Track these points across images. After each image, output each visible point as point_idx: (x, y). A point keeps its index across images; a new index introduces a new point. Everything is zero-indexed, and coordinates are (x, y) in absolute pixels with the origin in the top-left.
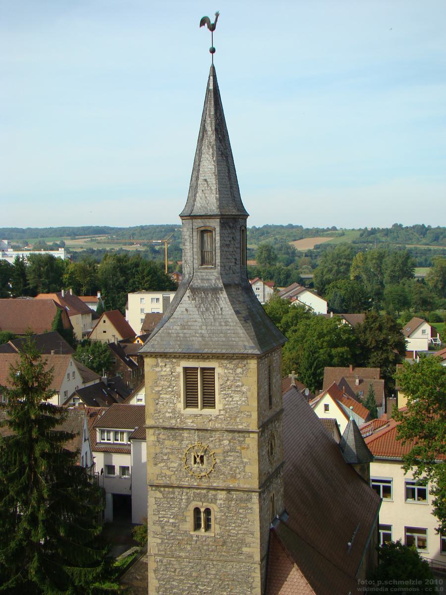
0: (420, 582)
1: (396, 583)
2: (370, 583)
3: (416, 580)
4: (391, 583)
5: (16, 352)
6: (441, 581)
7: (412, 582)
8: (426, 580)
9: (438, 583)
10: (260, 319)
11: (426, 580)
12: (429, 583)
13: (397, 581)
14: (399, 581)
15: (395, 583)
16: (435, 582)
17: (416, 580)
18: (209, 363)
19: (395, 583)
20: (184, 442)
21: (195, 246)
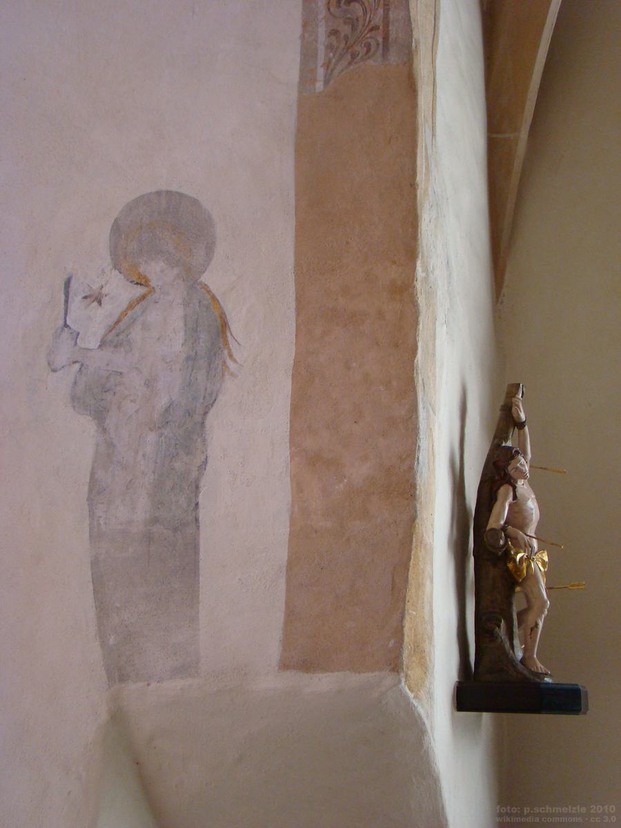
0: (584, 810)
1: (551, 811)
2: (503, 810)
3: (578, 806)
4: (543, 810)
5: (415, 40)
6: (612, 810)
7: (572, 809)
8: (592, 807)
9: (608, 810)
10: (520, 580)
11: (592, 807)
12: (596, 810)
13: (552, 807)
14: (554, 808)
15: (549, 810)
16: (604, 810)
17: (570, 807)
18: (436, 534)
19: (549, 810)
20: (181, 502)
21: (421, 382)
